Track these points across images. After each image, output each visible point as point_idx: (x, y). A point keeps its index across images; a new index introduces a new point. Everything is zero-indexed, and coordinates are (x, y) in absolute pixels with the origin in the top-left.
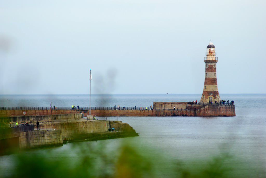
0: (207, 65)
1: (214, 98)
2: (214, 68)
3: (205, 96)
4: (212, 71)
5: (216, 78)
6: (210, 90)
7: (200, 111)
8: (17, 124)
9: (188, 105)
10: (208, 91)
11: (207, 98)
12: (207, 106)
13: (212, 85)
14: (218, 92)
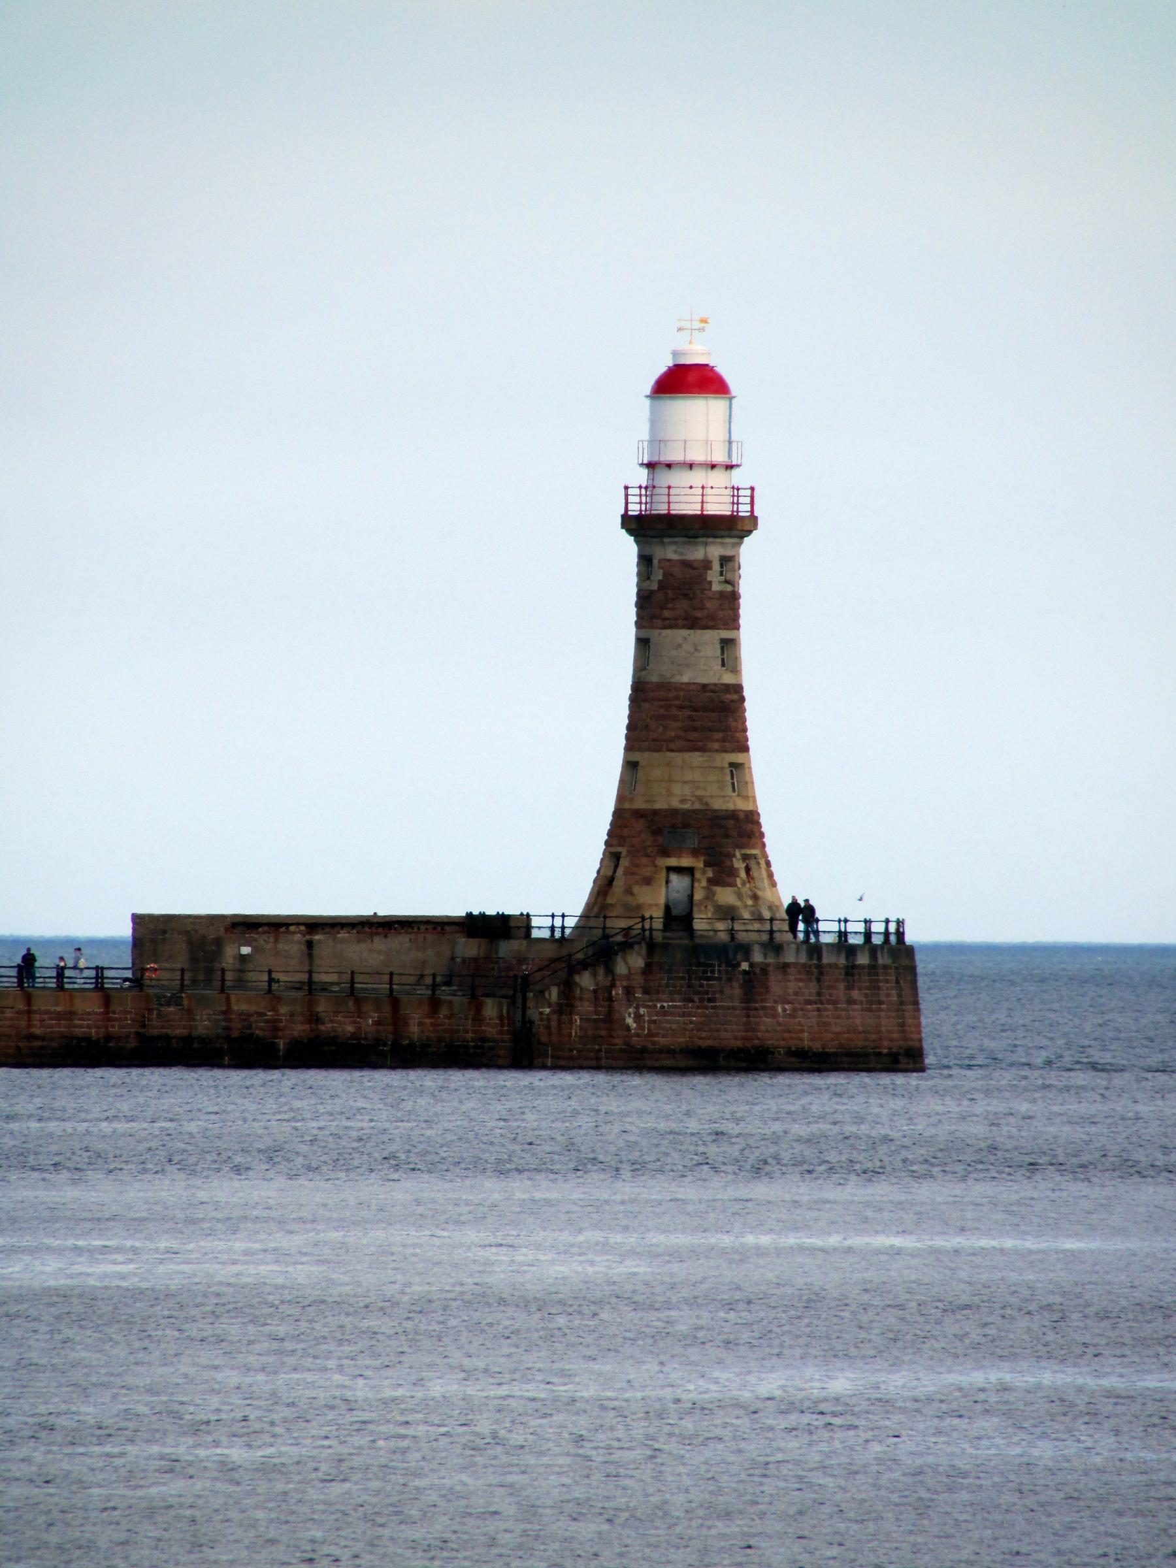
0: (645, 560)
1: (713, 882)
2: (716, 587)
3: (624, 862)
4: (692, 623)
5: (738, 689)
6: (675, 804)
7: (566, 1006)
8: (148, 944)
9: (468, 948)
10: (655, 812)
11: (648, 881)
12: (636, 960)
13: (696, 758)
14: (752, 818)
